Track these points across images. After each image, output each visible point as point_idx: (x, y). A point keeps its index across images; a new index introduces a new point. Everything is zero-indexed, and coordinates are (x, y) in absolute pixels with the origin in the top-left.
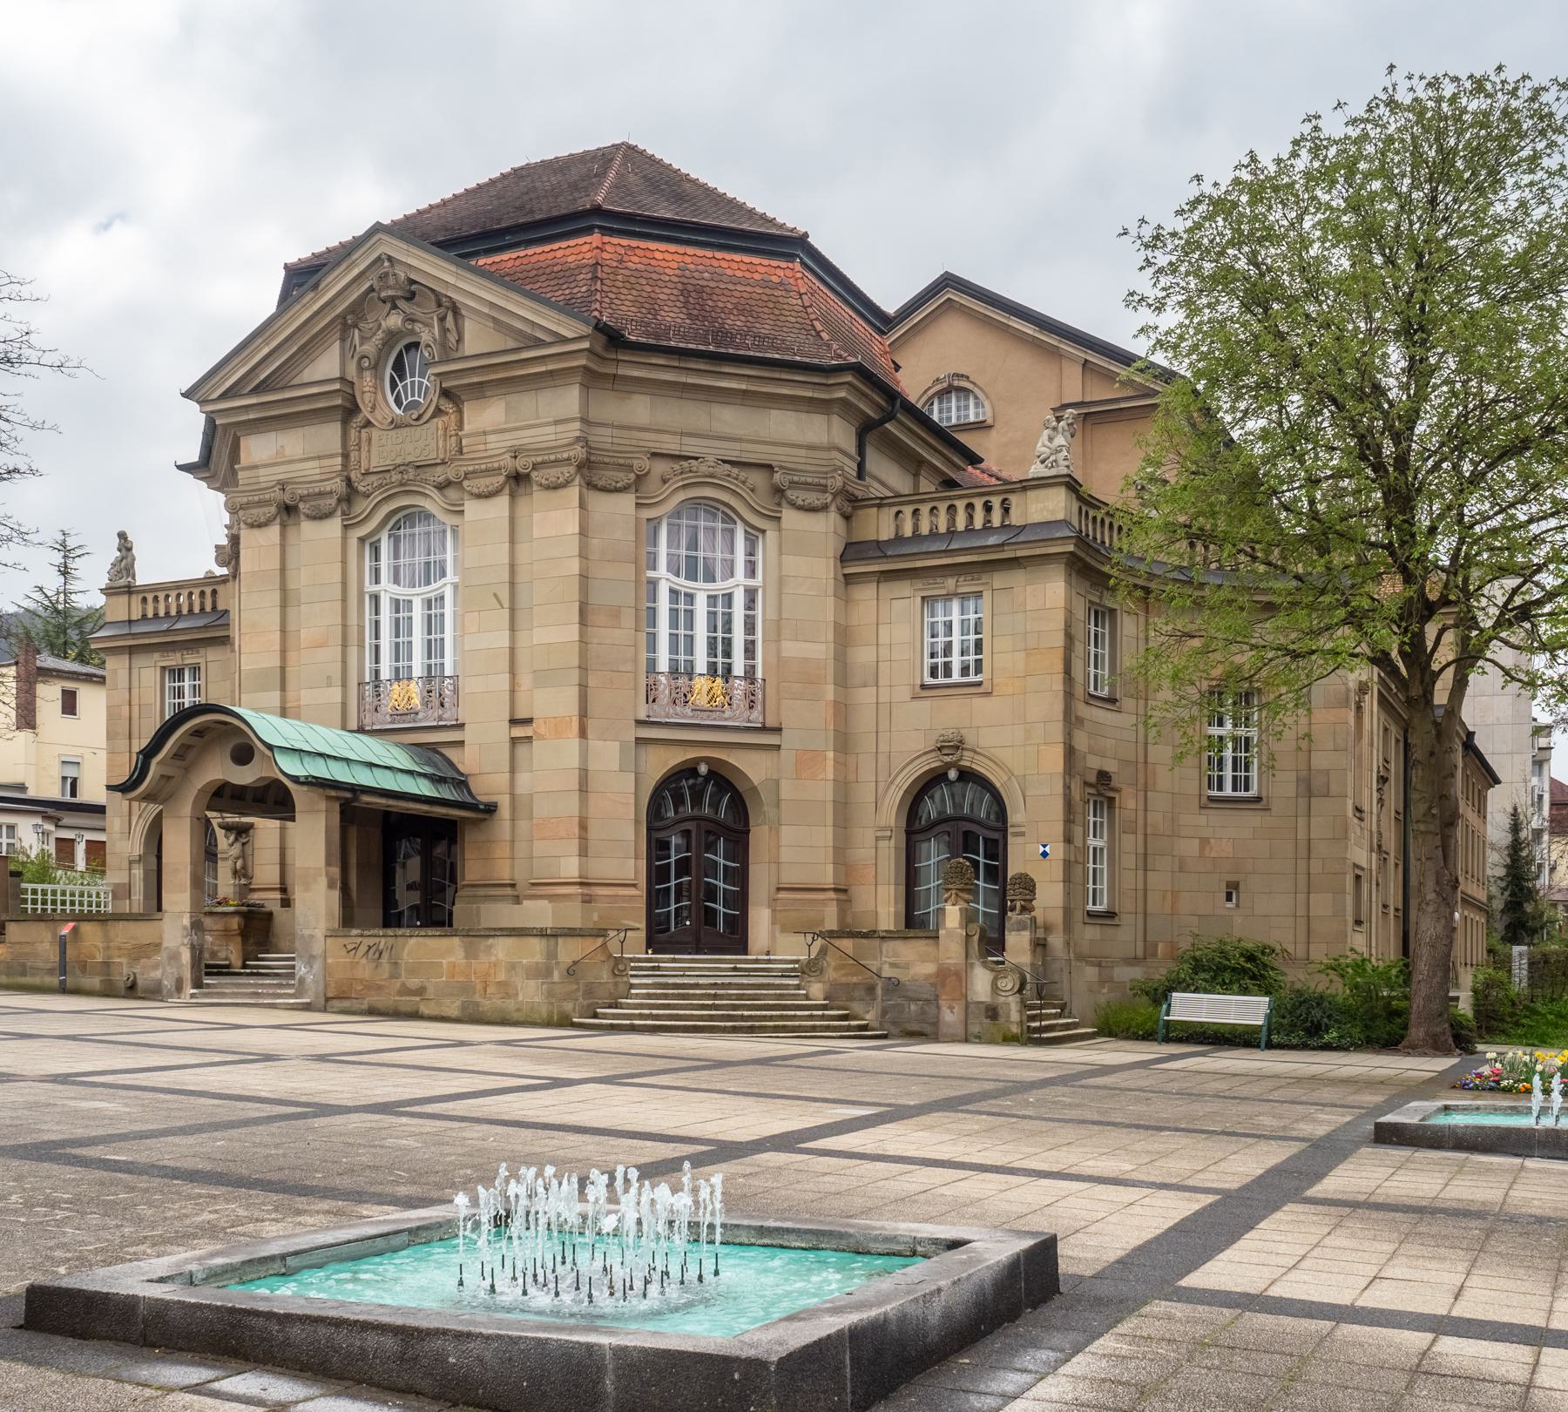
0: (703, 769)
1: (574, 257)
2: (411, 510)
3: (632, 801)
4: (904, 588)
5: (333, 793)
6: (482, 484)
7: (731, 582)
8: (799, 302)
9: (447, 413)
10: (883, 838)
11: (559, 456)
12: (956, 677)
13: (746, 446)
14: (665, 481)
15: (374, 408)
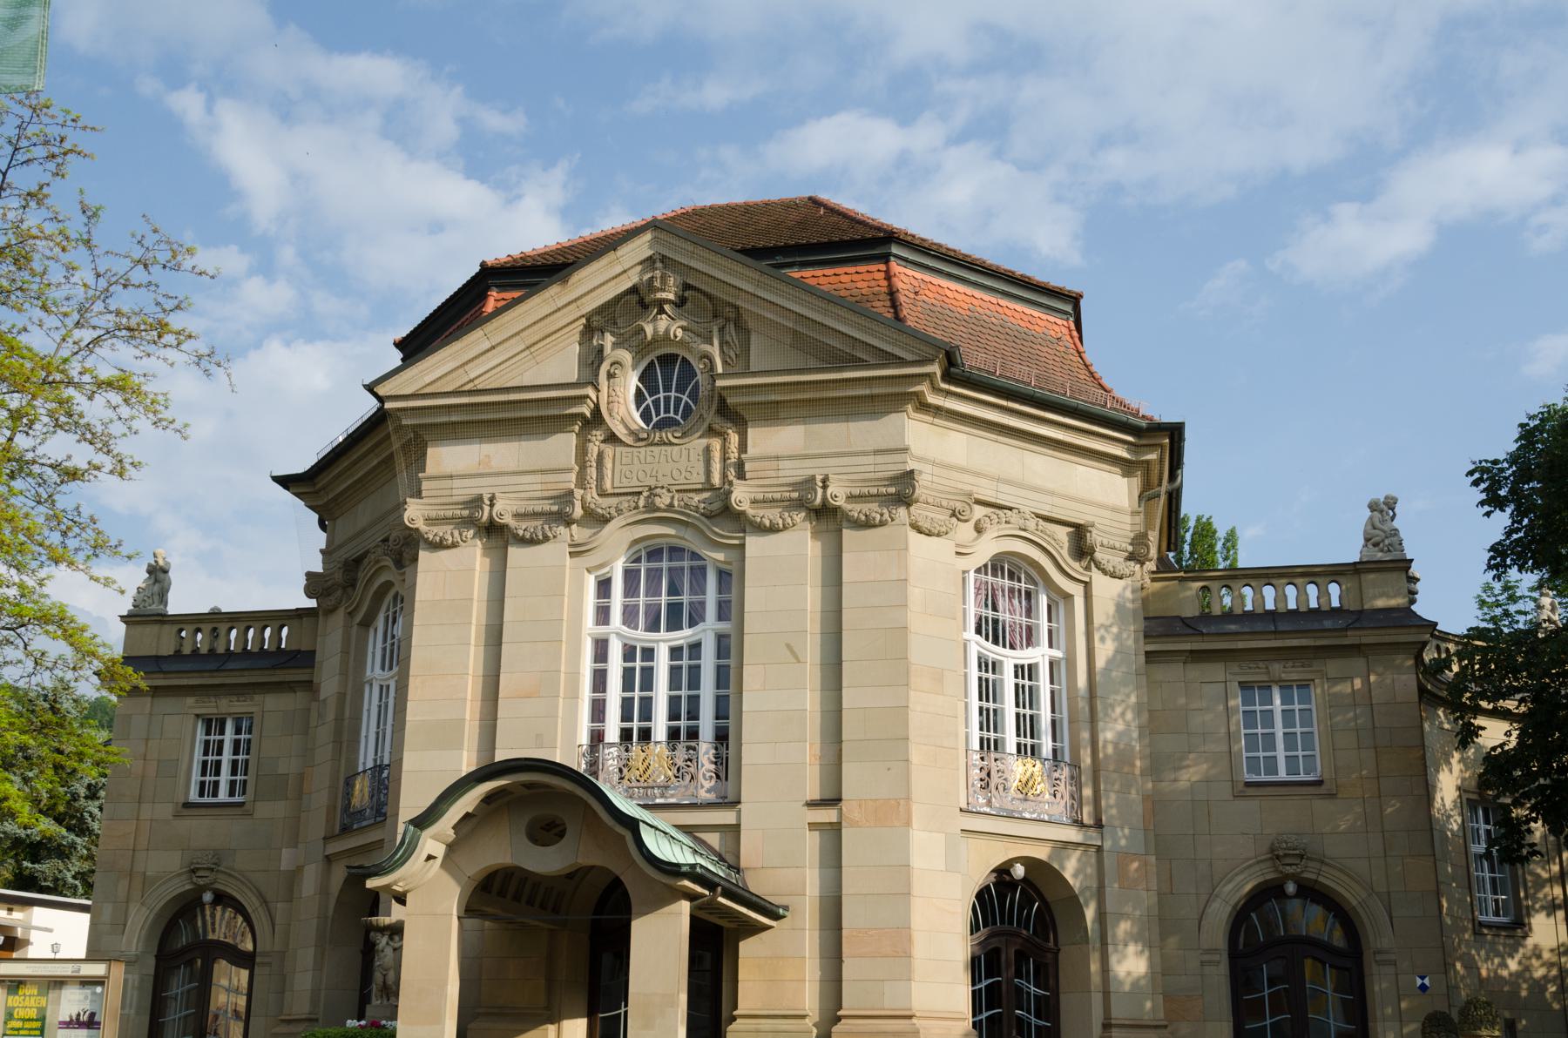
4: (1216, 671)
10: (1210, 963)
12: (1282, 775)
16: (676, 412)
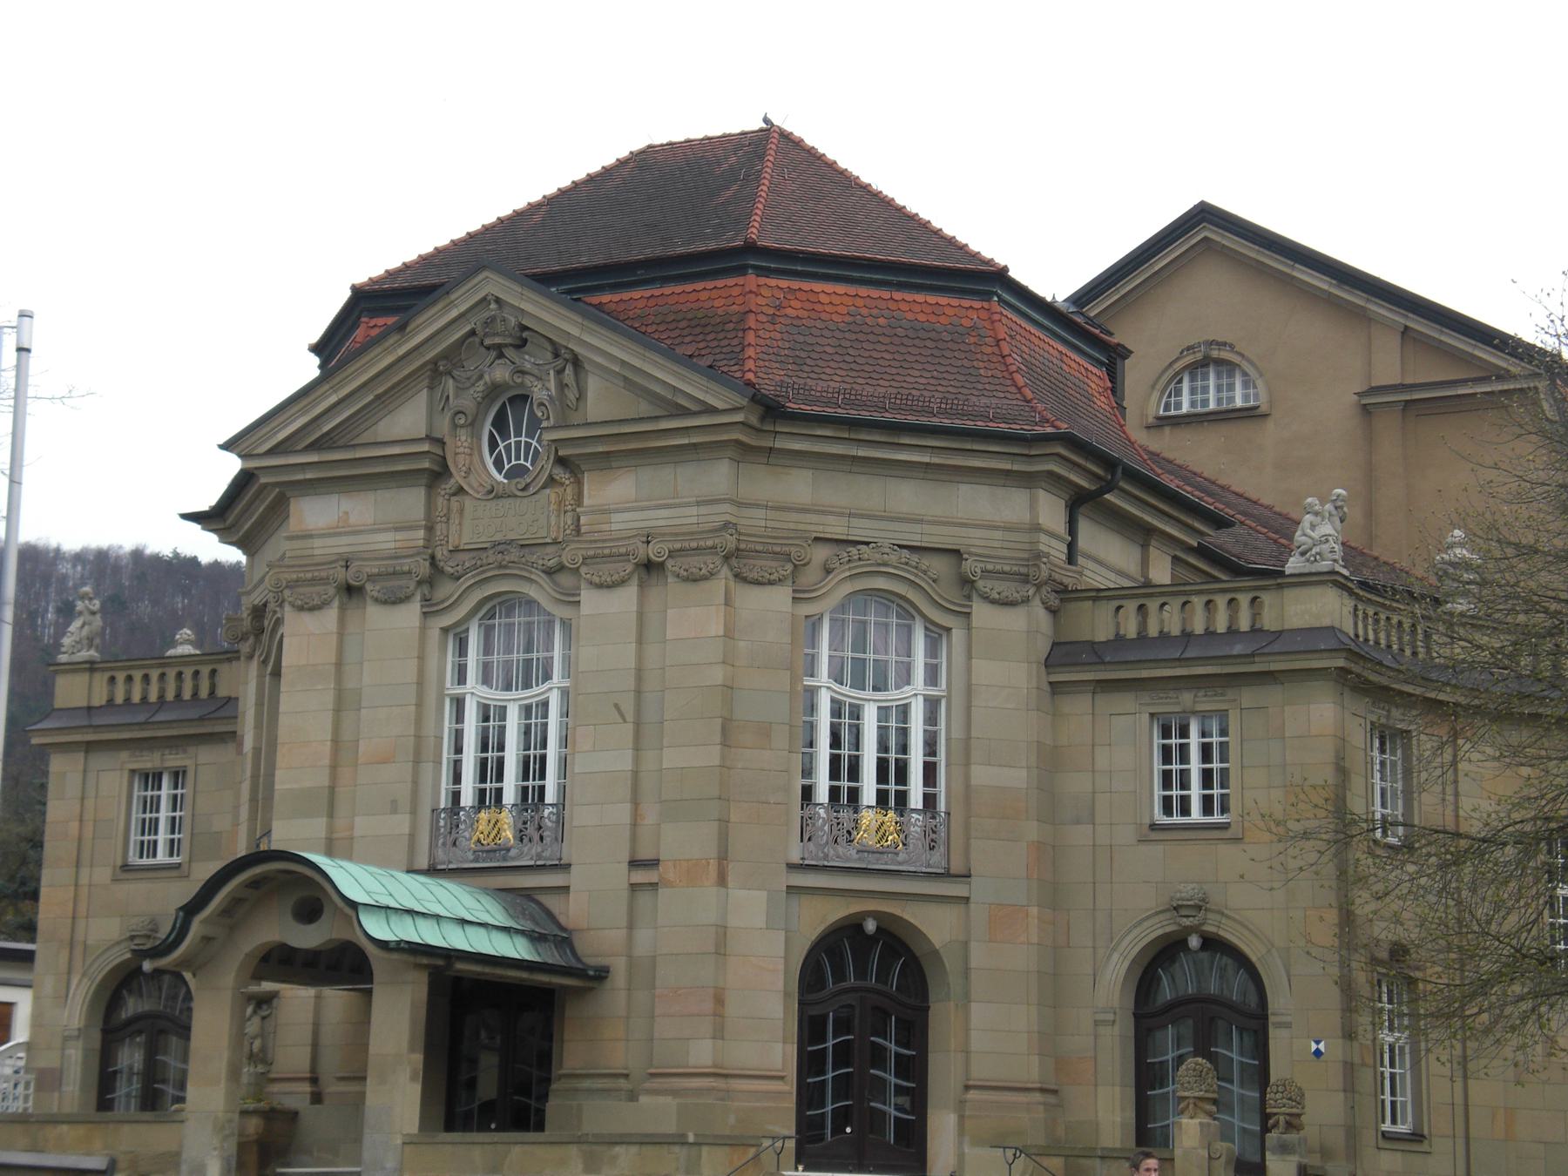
0: (871, 926)
1: (722, 302)
2: (511, 596)
3: (781, 967)
5: (425, 961)
6: (607, 571)
7: (907, 691)
8: (996, 350)
9: (562, 484)
10: (1104, 1023)
11: (702, 543)
13: (927, 528)
14: (828, 571)
15: (469, 471)
16: (526, 460)
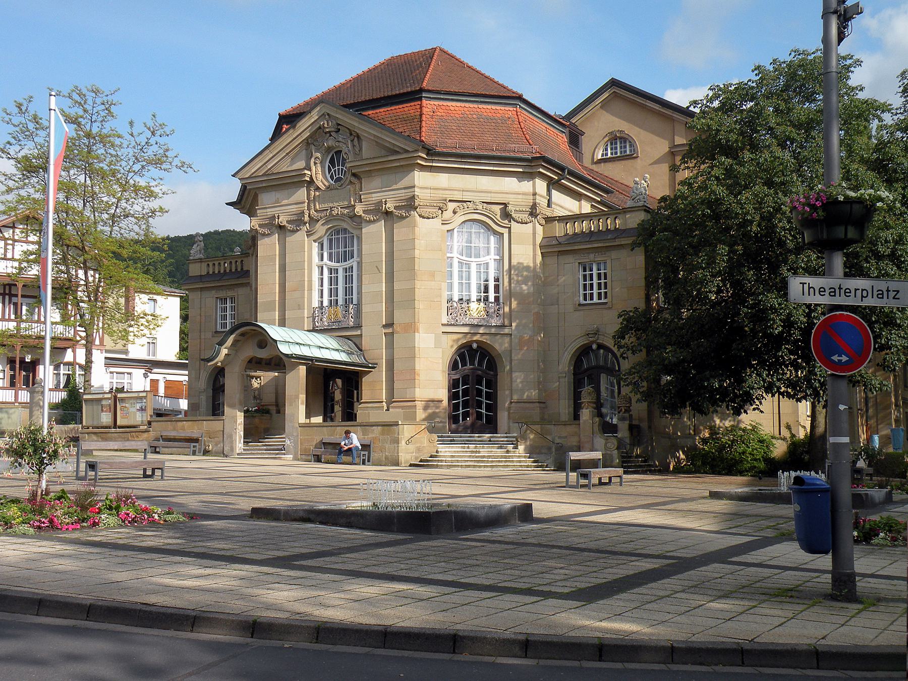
0: (475, 346)
4: (570, 259)
7: (487, 258)
13: (493, 195)
